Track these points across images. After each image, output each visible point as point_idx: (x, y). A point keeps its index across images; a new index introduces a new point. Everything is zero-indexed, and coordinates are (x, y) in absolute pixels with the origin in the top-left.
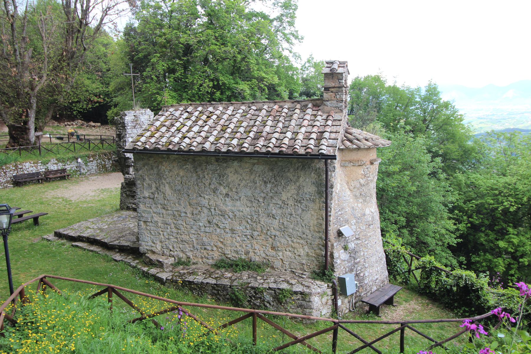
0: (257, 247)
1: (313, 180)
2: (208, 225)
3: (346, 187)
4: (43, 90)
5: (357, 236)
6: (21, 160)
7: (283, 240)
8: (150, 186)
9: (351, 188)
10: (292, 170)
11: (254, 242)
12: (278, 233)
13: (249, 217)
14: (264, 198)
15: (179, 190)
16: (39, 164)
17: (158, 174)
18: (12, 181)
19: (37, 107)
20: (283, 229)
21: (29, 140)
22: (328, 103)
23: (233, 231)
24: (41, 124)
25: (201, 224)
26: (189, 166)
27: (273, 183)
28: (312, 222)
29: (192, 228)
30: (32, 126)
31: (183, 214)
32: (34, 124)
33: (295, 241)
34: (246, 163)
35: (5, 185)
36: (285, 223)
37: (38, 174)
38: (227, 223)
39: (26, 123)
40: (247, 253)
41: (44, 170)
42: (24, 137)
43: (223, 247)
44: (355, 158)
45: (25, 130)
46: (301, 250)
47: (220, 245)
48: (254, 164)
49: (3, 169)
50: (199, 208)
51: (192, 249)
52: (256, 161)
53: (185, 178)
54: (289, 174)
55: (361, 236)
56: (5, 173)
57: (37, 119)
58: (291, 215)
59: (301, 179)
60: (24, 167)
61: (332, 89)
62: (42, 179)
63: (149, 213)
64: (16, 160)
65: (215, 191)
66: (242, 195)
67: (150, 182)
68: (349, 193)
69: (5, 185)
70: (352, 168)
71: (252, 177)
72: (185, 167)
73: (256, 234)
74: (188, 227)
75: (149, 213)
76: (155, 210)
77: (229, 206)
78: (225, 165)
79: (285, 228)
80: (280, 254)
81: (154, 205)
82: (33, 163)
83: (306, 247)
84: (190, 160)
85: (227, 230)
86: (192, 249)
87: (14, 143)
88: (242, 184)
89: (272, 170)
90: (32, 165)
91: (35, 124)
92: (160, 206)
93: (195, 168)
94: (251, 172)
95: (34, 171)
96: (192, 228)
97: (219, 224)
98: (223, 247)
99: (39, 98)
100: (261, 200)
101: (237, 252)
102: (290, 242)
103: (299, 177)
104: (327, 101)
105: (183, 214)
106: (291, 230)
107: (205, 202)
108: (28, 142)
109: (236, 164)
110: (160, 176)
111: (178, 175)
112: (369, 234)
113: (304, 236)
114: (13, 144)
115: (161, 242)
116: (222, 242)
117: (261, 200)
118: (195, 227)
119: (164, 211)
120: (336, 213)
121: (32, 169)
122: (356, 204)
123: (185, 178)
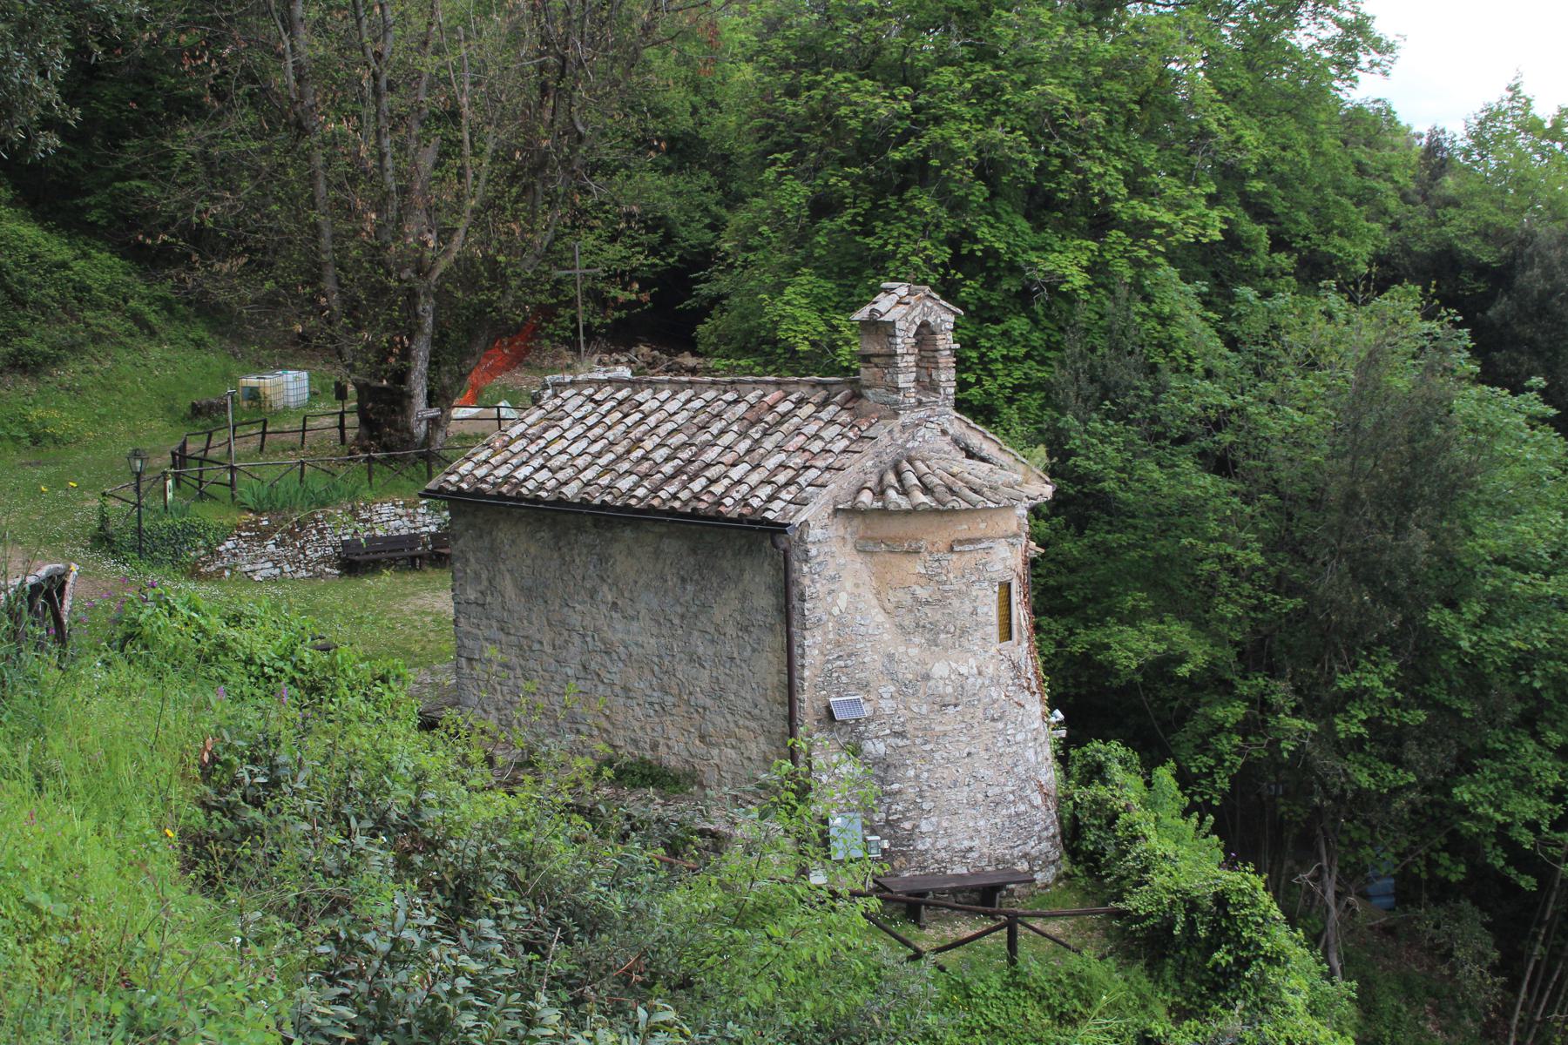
0: (673, 732)
1: (769, 580)
2: (582, 674)
3: (875, 602)
4: (446, 275)
5: (897, 728)
6: (369, 495)
7: (719, 720)
8: (477, 576)
9: (889, 606)
10: (729, 553)
11: (667, 719)
12: (709, 702)
13: (656, 660)
14: (683, 617)
15: (530, 589)
16: (421, 510)
17: (492, 549)
18: (339, 557)
19: (436, 324)
20: (718, 693)
21: (408, 430)
22: (869, 393)
23: (626, 689)
24: (446, 381)
25: (570, 672)
26: (545, 534)
27: (697, 583)
28: (769, 680)
29: (553, 679)
30: (419, 387)
31: (536, 646)
32: (424, 382)
33: (741, 723)
34: (647, 531)
35: (318, 568)
36: (722, 678)
37: (413, 539)
38: (615, 672)
39: (401, 376)
40: (654, 747)
41: (433, 529)
42: (395, 421)
43: (610, 728)
44: (901, 533)
45: (397, 399)
46: (753, 745)
47: (605, 724)
48: (661, 536)
49: (316, 521)
50: (566, 633)
51: (553, 729)
52: (664, 530)
53: (539, 562)
54: (725, 564)
55: (909, 727)
56: (320, 531)
57: (434, 364)
58: (732, 659)
59: (747, 576)
60: (375, 518)
61: (876, 360)
62: (421, 557)
63: (476, 638)
64: (353, 496)
65: (592, 593)
66: (641, 606)
67: (478, 567)
68: (881, 617)
69: (318, 568)
70: (887, 556)
71: (660, 566)
72: (538, 536)
73: (669, 700)
74: (547, 676)
75: (476, 638)
76: (487, 633)
77: (618, 632)
78: (609, 535)
79: (722, 690)
80: (715, 752)
81: (485, 622)
82: (404, 506)
83: (762, 739)
84: (548, 521)
85: (617, 689)
86: (553, 729)
87: (371, 438)
88: (641, 582)
89: (694, 551)
90: (400, 511)
91: (430, 379)
92: (495, 624)
93: (557, 538)
94: (657, 554)
95: (404, 532)
96: (553, 679)
97: (603, 674)
98: (610, 728)
99: (442, 297)
100: (676, 621)
101: (635, 742)
102: (732, 725)
103: (742, 571)
104: (868, 387)
105: (536, 646)
106: (732, 697)
107: (575, 620)
108: (408, 442)
109: (628, 533)
110: (494, 553)
111: (527, 551)
112: (938, 728)
113: (757, 711)
114: (366, 443)
115: (497, 709)
116: (607, 717)
117: (676, 621)
118: (558, 677)
119: (502, 636)
120: (828, 661)
121: (398, 523)
122: (902, 649)
123: (539, 562)
